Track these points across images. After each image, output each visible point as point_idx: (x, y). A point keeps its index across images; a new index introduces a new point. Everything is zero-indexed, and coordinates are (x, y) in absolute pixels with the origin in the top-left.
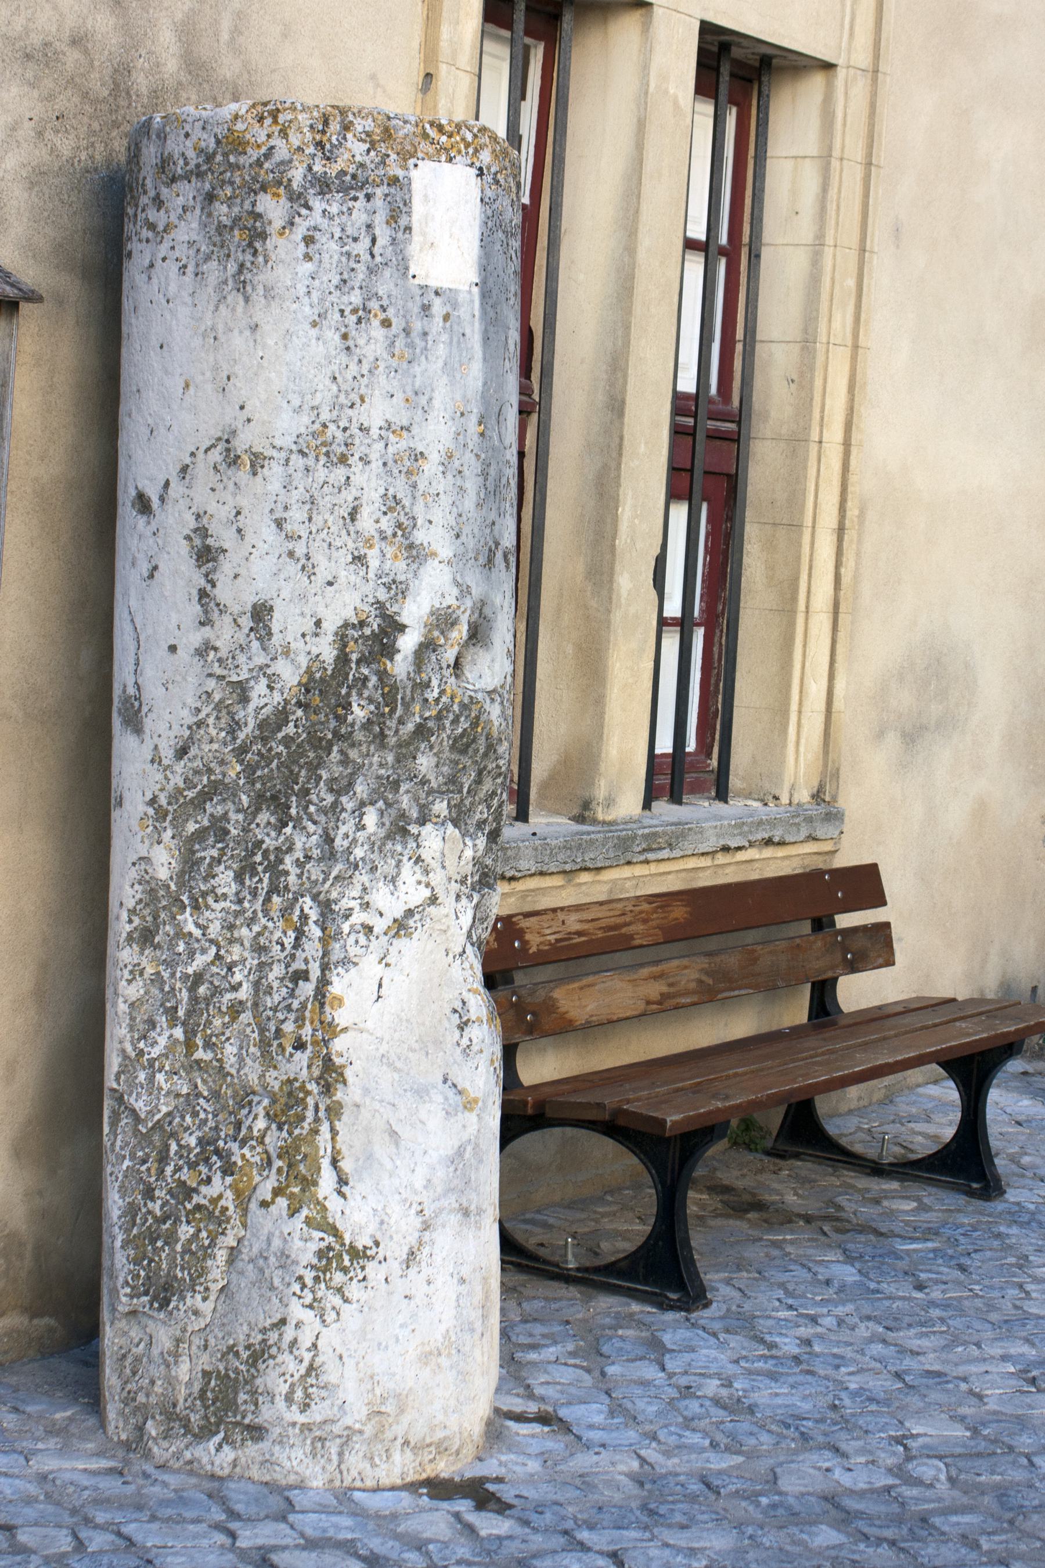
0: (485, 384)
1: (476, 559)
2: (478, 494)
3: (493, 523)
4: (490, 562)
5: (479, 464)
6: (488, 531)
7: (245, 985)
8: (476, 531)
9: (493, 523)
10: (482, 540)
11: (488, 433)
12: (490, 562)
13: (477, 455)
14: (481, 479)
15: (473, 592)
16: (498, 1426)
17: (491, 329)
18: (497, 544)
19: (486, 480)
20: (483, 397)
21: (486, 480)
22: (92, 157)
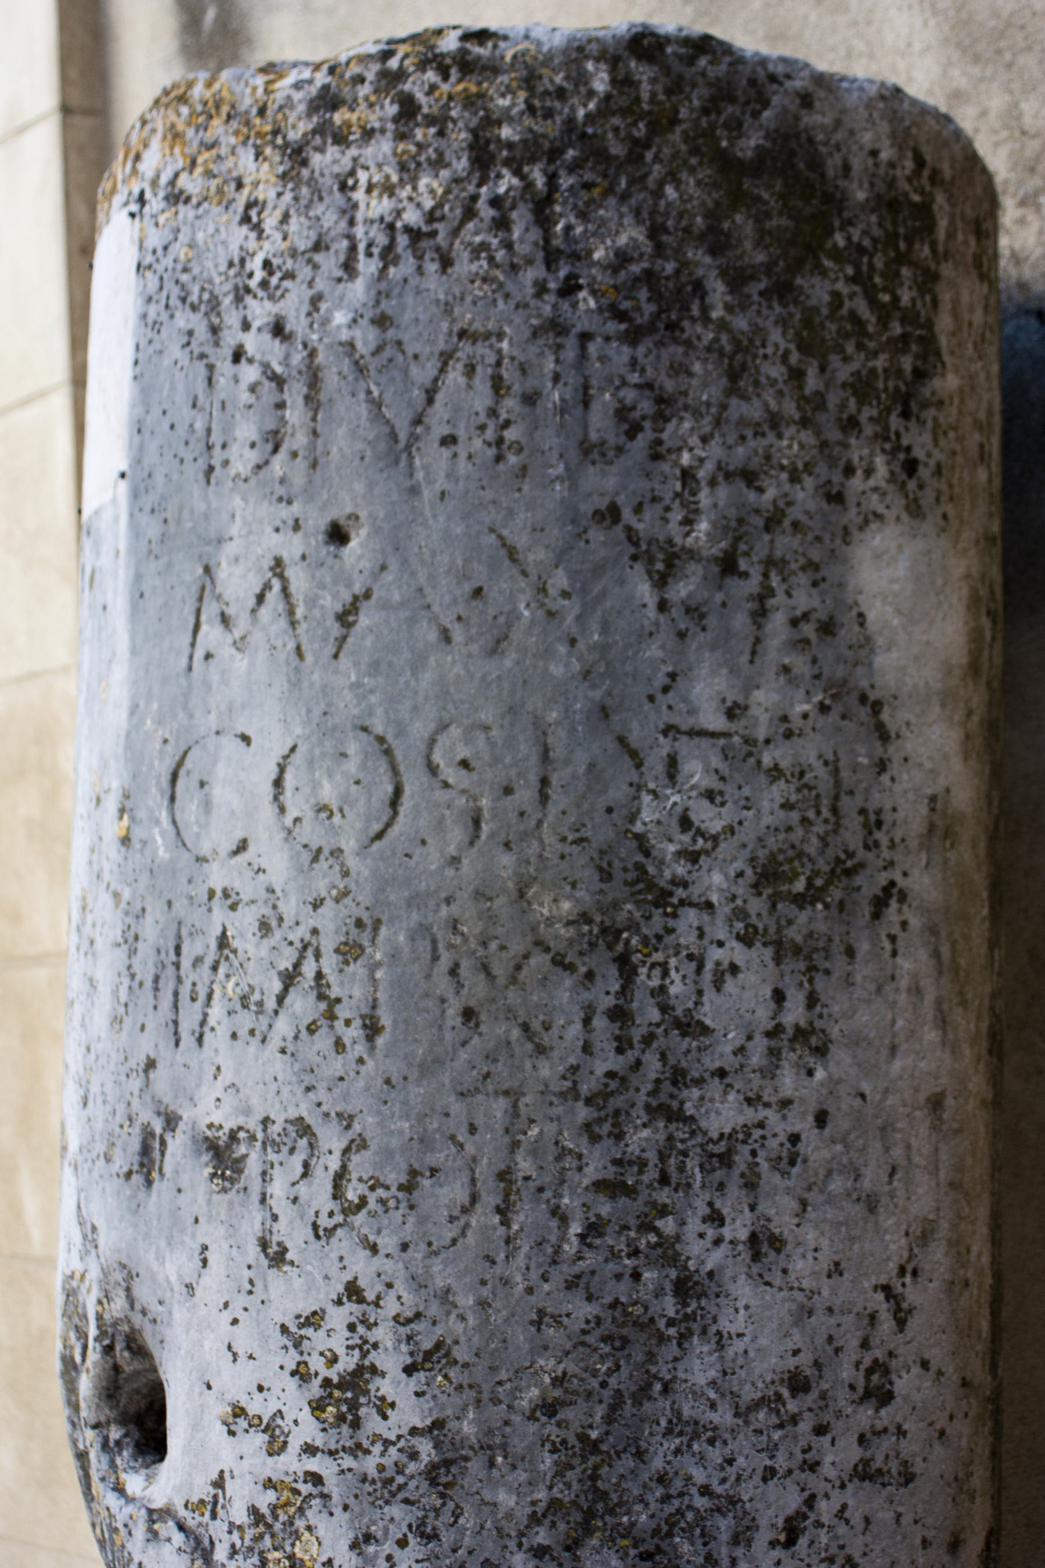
0: (134, 710)
1: (108, 1159)
2: (115, 992)
3: (151, 1064)
4: (147, 1162)
5: (120, 913)
6: (135, 1084)
7: (410, 1536)
8: (109, 1086)
9: (151, 1064)
10: (121, 1108)
11: (137, 834)
12: (147, 1162)
13: (116, 895)
14: (122, 953)
15: (102, 1241)
16: (871, 518)
17: (152, 567)
18: (171, 1121)
19: (133, 952)
20: (128, 747)
21: (133, 952)
22: (710, 1354)
